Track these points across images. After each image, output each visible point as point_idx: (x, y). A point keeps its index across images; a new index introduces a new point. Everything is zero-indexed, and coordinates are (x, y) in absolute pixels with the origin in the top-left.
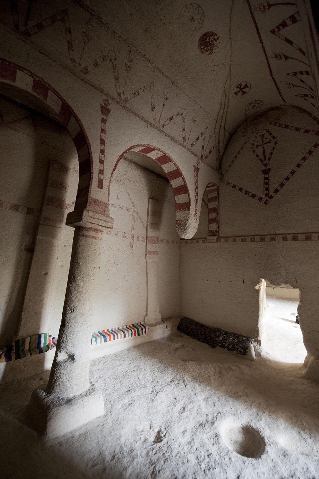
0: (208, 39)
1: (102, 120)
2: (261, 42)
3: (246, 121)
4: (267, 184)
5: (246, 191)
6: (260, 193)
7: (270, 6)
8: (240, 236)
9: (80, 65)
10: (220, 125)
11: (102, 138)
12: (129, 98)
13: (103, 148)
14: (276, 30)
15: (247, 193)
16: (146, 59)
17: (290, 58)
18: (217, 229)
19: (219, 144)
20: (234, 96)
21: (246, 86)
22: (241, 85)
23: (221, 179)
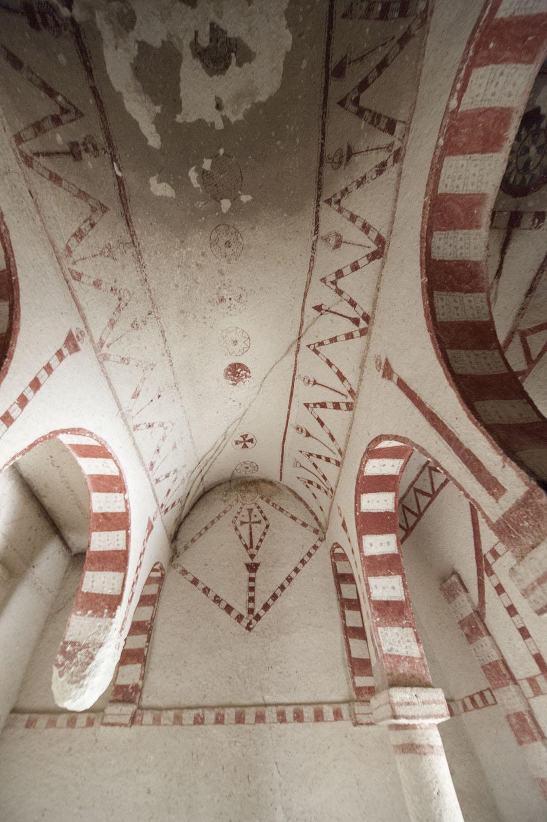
0: (239, 370)
1: (58, 351)
2: (289, 408)
3: (230, 481)
4: (252, 589)
5: (216, 596)
6: (240, 608)
7: (315, 383)
8: (189, 708)
9: (74, 263)
10: (200, 471)
11: (39, 377)
12: (112, 358)
13: (29, 394)
14: (312, 405)
15: (217, 600)
16: (163, 335)
17: (313, 437)
18: (140, 683)
19: (187, 497)
20: (234, 444)
21: (251, 441)
22: (247, 436)
23: (172, 560)
